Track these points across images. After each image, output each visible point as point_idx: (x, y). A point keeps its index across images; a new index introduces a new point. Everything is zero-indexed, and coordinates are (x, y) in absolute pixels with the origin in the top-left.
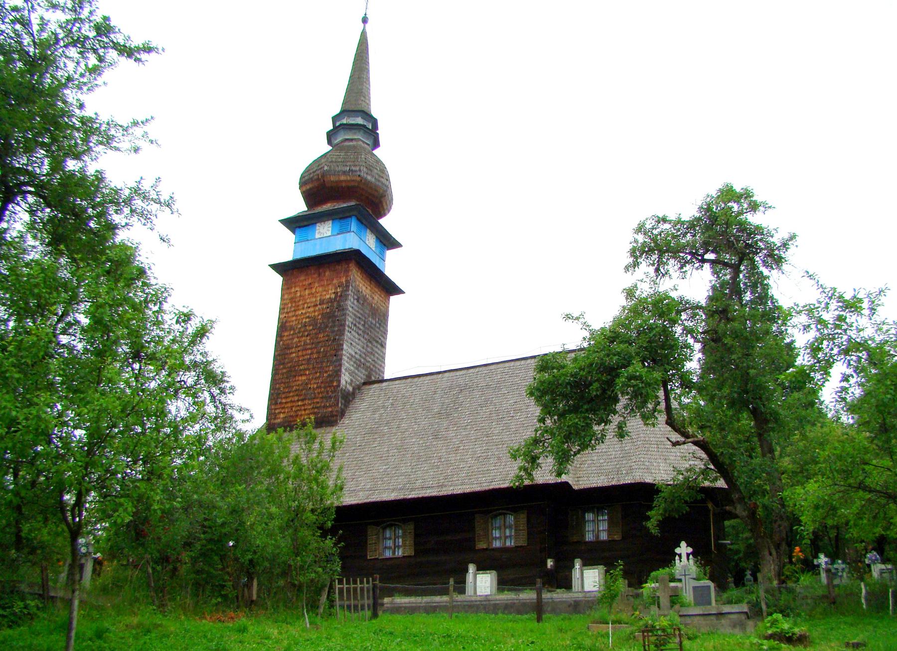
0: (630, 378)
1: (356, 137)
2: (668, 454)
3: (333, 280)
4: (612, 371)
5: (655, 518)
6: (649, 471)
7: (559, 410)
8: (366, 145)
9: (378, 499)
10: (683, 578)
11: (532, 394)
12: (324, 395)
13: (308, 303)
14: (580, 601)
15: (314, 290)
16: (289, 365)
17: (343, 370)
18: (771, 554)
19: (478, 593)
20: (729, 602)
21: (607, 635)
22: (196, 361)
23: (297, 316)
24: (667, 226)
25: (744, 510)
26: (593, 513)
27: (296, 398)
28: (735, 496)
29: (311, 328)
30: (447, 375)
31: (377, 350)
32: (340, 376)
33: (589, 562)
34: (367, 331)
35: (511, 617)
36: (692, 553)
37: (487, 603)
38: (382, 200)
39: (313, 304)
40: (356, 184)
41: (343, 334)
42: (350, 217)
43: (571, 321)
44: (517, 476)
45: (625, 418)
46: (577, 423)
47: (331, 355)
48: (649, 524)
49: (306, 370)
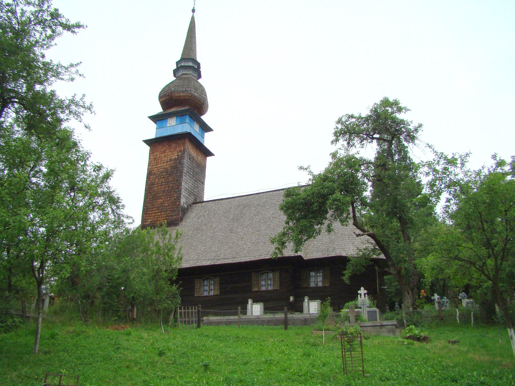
3: (176, 148)
4: (325, 197)
9: (201, 265)
10: (362, 306)
11: (282, 209)
12: (172, 209)
15: (166, 154)
16: (153, 193)
17: (182, 196)
18: (409, 294)
19: (254, 315)
20: (387, 319)
21: (322, 336)
23: (157, 167)
24: (354, 120)
25: (395, 270)
26: (315, 272)
27: (157, 211)
28: (390, 263)
29: (165, 174)
30: (237, 199)
32: (180, 199)
35: (271, 327)
40: (189, 98)
41: (182, 177)
42: (186, 115)
43: (302, 170)
44: (274, 253)
45: (331, 222)
46: (306, 224)
48: (344, 278)
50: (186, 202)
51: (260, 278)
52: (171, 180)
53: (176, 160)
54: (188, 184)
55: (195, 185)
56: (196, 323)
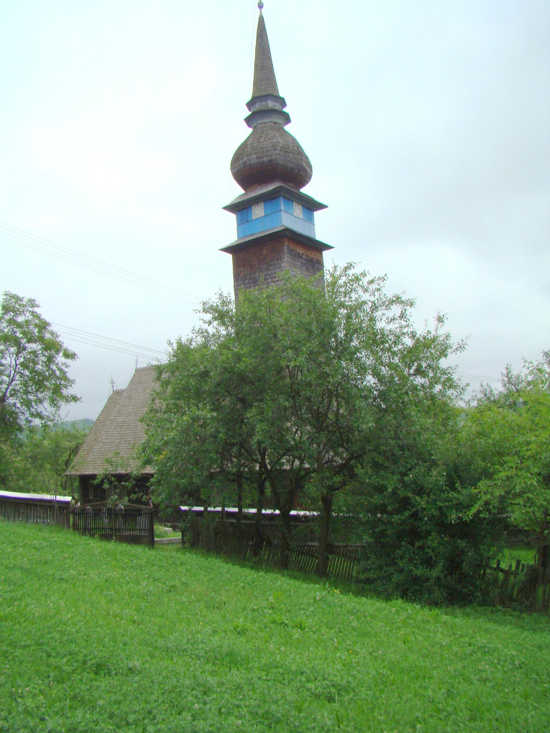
22: (427, 530)
42: (277, 197)
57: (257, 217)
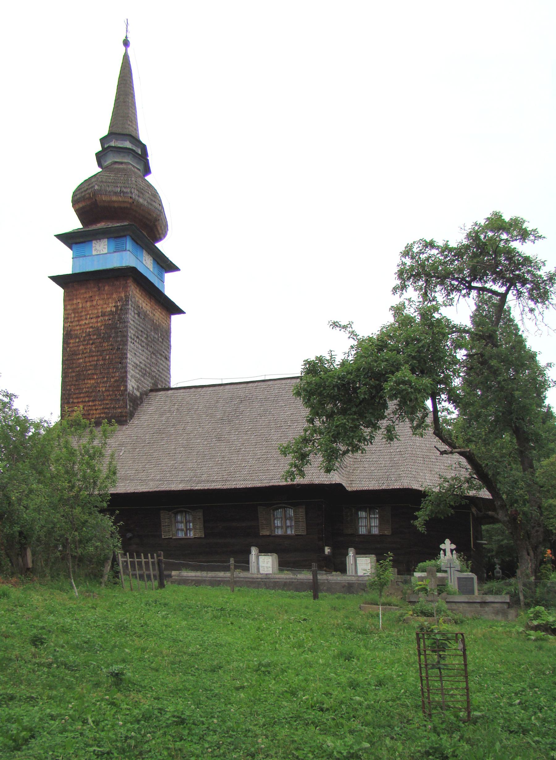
0: (398, 383)
1: (126, 161)
2: (433, 466)
3: (112, 294)
4: (381, 377)
5: (423, 517)
6: (416, 479)
7: (327, 411)
8: (136, 170)
9: (168, 489)
10: (448, 569)
11: (298, 394)
12: (113, 397)
13: (90, 315)
14: (353, 583)
15: (95, 303)
16: (78, 369)
17: (129, 377)
18: (528, 554)
19: (261, 572)
20: (490, 592)
21: (378, 615)
23: (80, 325)
24: (434, 252)
25: (506, 516)
26: (366, 512)
27: (87, 399)
28: (498, 503)
29: (95, 337)
30: (228, 387)
31: (162, 362)
32: (126, 382)
33: (361, 551)
34: (150, 344)
35: (289, 593)
36: (455, 549)
37: (268, 580)
38: (157, 223)
39: (95, 316)
40: (129, 206)
41: (126, 345)
42: (125, 236)
43: (338, 329)
44: (288, 472)
45: (393, 422)
46: (345, 424)
47: (117, 363)
48: (416, 523)
49: (93, 374)
50: (138, 387)
51: (272, 515)
52: (106, 348)
53: (113, 315)
54: (139, 357)
55: (153, 360)
56: (155, 579)
57: (99, 253)
